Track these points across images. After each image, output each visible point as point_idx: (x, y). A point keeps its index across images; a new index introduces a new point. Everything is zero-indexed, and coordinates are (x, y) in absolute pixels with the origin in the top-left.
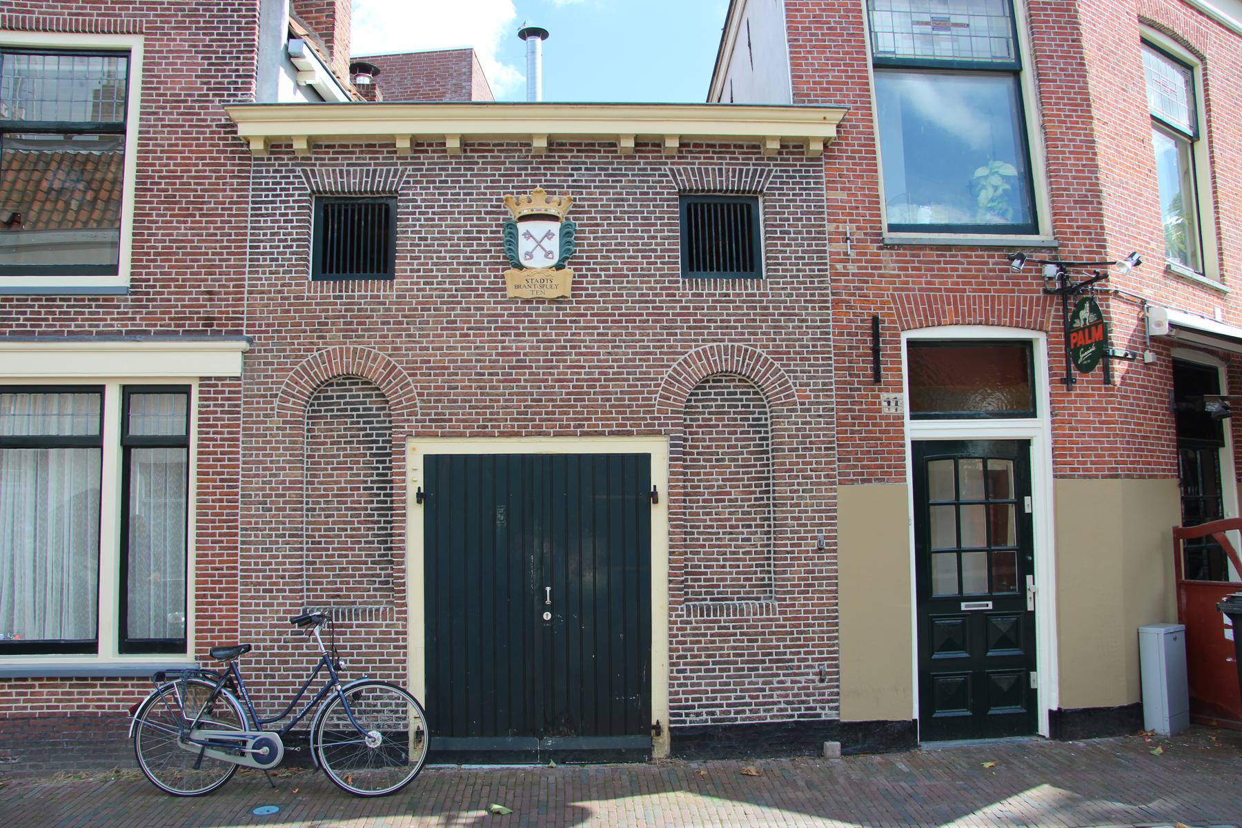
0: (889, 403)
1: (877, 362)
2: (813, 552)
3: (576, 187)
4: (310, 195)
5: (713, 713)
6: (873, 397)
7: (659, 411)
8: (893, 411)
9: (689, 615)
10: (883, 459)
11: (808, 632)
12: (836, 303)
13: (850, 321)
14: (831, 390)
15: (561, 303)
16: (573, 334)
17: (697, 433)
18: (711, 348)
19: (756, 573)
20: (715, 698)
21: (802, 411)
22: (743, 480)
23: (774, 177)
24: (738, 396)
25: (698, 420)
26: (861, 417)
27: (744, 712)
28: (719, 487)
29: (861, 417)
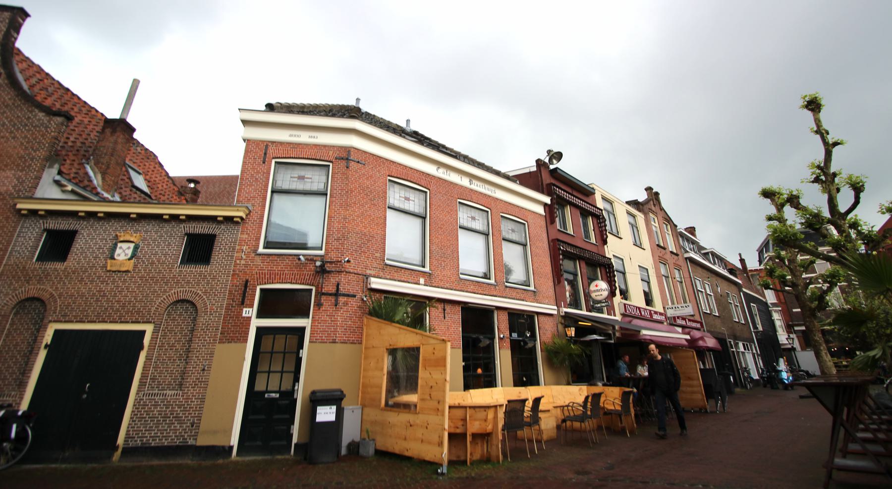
3: (146, 232)
12: (233, 275)
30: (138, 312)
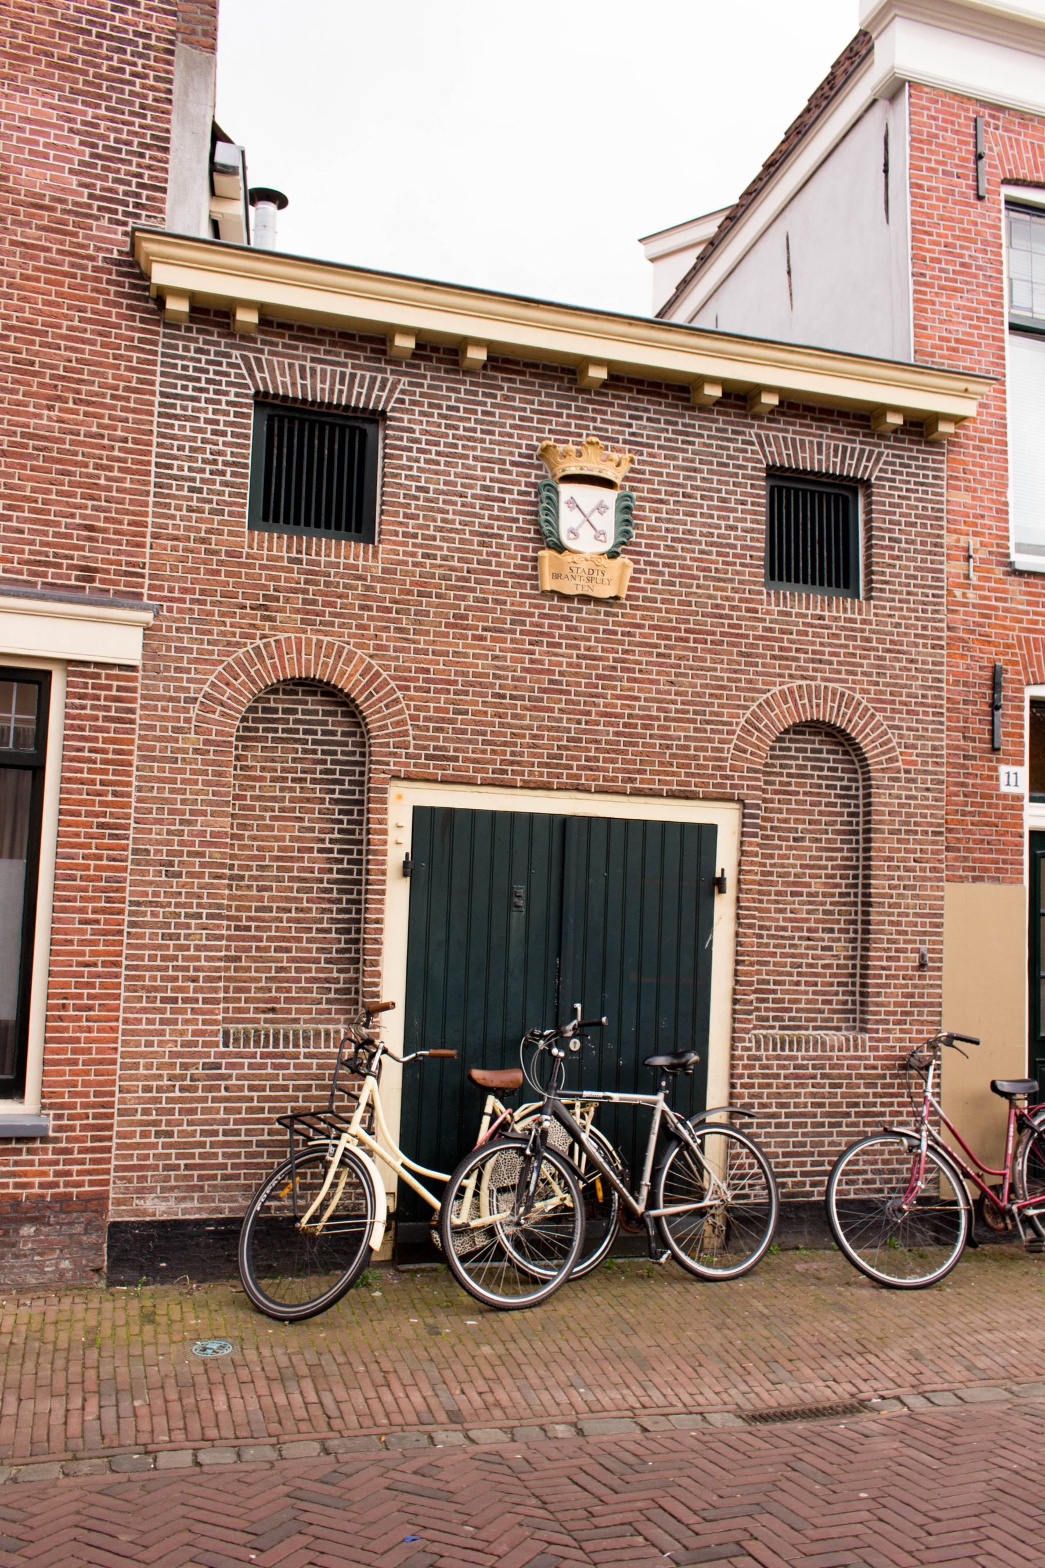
6: (990, 769)
9: (758, 1048)
17: (772, 801)
21: (908, 780)
22: (825, 867)
30: (685, 760)
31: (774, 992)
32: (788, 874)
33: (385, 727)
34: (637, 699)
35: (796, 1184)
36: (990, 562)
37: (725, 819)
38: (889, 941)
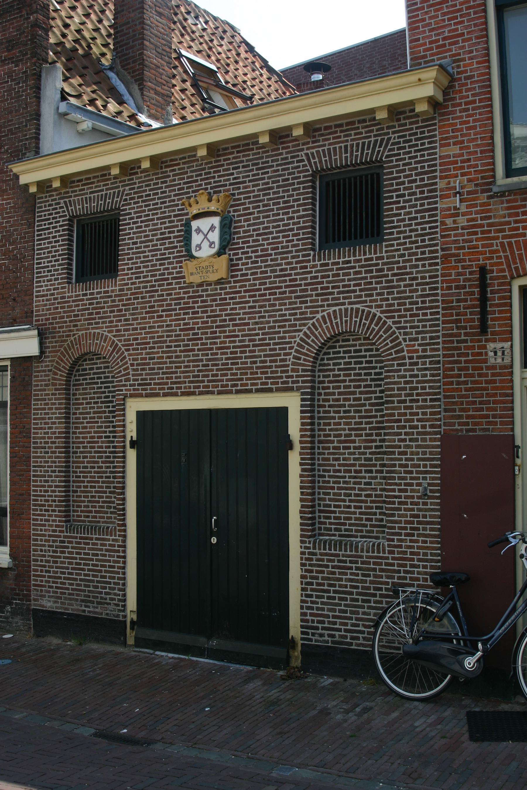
0: (495, 353)
1: (484, 313)
2: (419, 497)
4: (312, 175)
5: (333, 636)
6: (479, 347)
7: (293, 370)
8: (499, 360)
9: (314, 548)
10: (488, 409)
11: (413, 572)
12: (445, 258)
13: (458, 274)
14: (438, 343)
15: (223, 283)
16: (232, 309)
17: (328, 388)
18: (335, 311)
19: (375, 514)
20: (335, 623)
21: (411, 364)
22: (365, 429)
23: (393, 144)
24: (363, 353)
25: (329, 376)
26: (467, 369)
27: (358, 638)
28: (346, 436)
29: (467, 369)
31: (335, 512)
32: (340, 435)
33: (120, 372)
34: (237, 336)
35: (341, 636)
36: (476, 192)
37: (134, 406)
38: (400, 478)
